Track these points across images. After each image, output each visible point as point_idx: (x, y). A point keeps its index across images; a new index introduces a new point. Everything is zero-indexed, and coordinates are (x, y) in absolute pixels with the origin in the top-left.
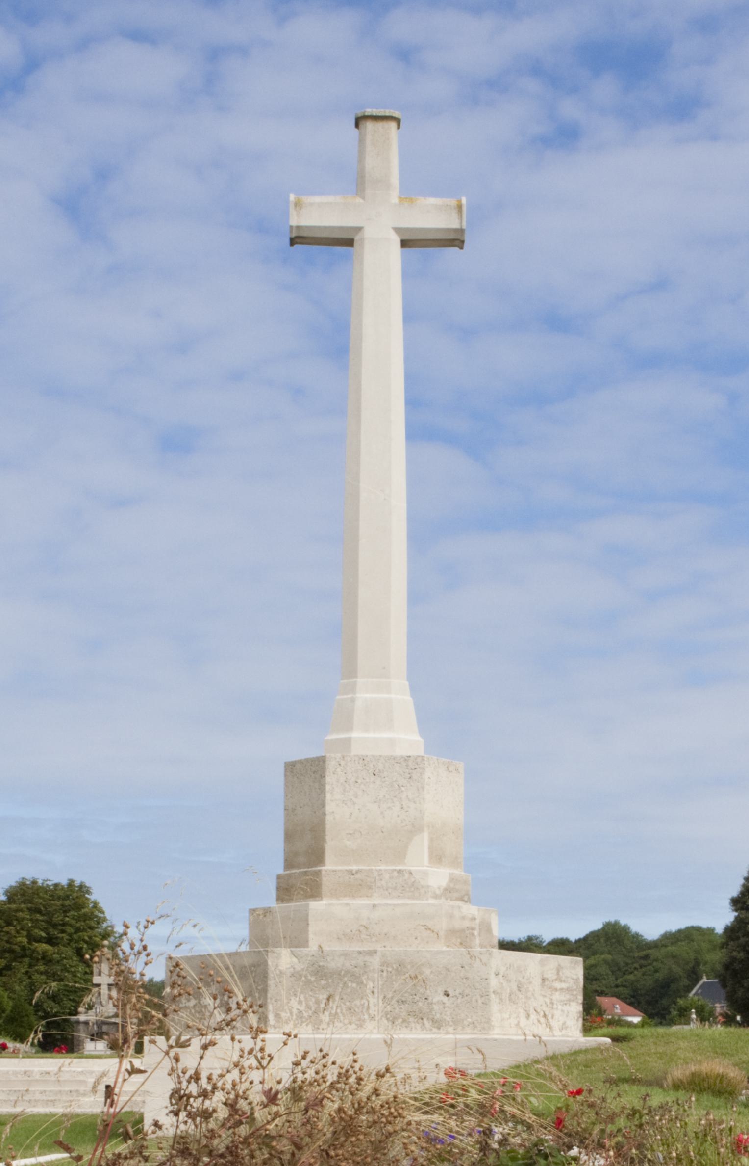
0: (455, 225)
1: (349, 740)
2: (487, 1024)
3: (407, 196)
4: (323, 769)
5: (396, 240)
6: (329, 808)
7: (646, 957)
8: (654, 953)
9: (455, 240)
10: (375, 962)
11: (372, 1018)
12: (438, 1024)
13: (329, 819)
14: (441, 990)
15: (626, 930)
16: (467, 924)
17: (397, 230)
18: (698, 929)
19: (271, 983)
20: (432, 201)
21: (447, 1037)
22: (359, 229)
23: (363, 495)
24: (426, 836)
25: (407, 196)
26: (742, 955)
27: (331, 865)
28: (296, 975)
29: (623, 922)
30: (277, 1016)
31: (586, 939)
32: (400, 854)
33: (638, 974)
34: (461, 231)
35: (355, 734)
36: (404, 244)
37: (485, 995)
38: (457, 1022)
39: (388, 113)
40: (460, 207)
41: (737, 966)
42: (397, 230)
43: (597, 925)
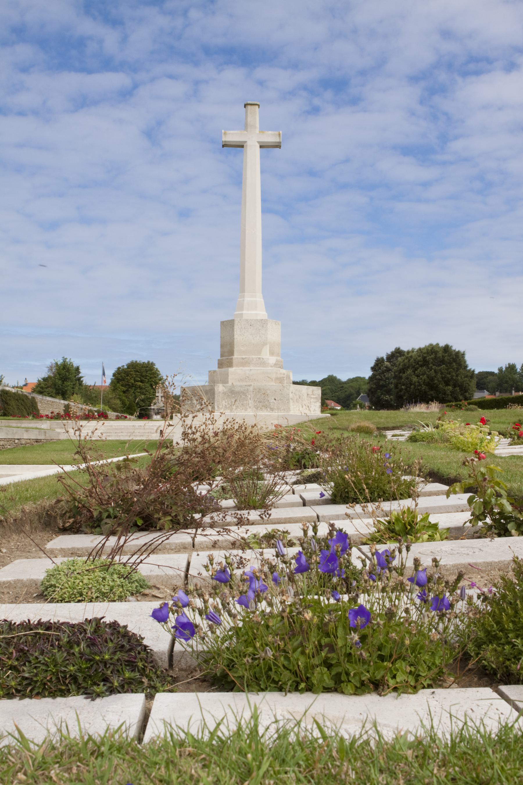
0: (278, 140)
1: (242, 314)
2: (289, 409)
3: (262, 131)
4: (234, 324)
5: (258, 146)
6: (236, 337)
7: (342, 387)
8: (345, 386)
9: (278, 146)
10: (251, 389)
11: (250, 407)
12: (272, 409)
13: (235, 340)
14: (273, 398)
15: (335, 378)
16: (282, 376)
17: (258, 142)
18: (360, 378)
19: (216, 396)
20: (270, 132)
21: (275, 414)
22: (245, 142)
23: (247, 232)
24: (268, 346)
25: (262, 131)
26: (374, 386)
27: (236, 356)
28: (224, 393)
29: (334, 375)
30: (218, 407)
31: (322, 381)
32: (260, 352)
33: (340, 392)
34: (280, 142)
35: (244, 312)
36: (261, 147)
37: (288, 400)
38: (278, 409)
39: (255, 103)
40: (279, 134)
41: (373, 390)
42: (259, 142)
43: (326, 376)
